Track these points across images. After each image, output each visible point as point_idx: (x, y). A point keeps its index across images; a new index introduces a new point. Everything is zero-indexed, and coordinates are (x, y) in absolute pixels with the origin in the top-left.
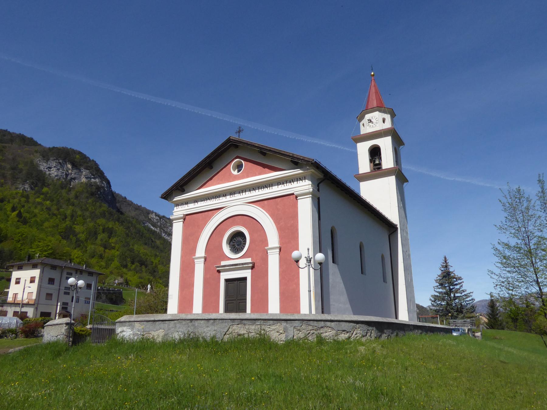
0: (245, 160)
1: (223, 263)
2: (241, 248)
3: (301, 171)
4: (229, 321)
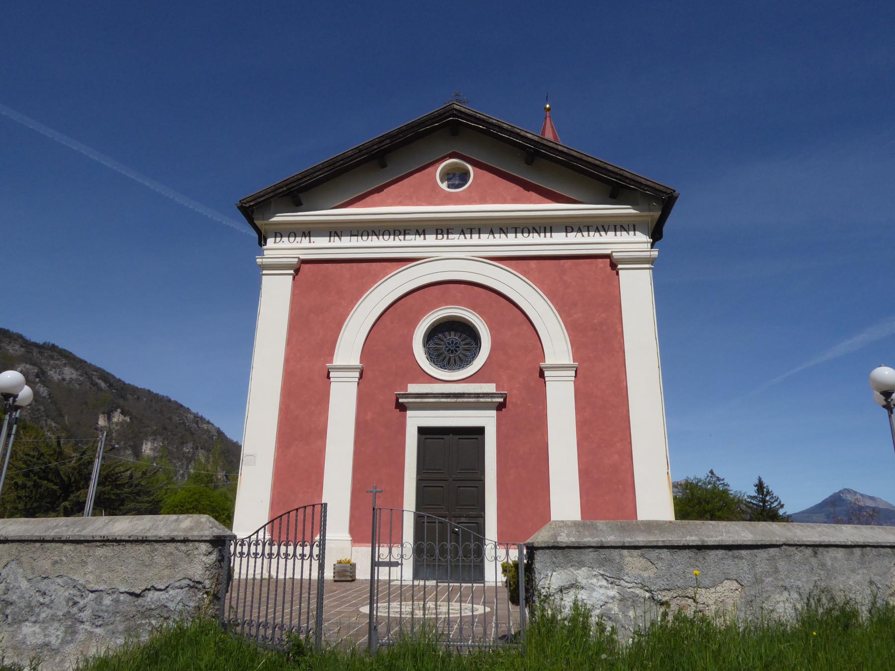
1: (413, 388)
2: (457, 358)
3: (632, 211)
4: (889, 550)
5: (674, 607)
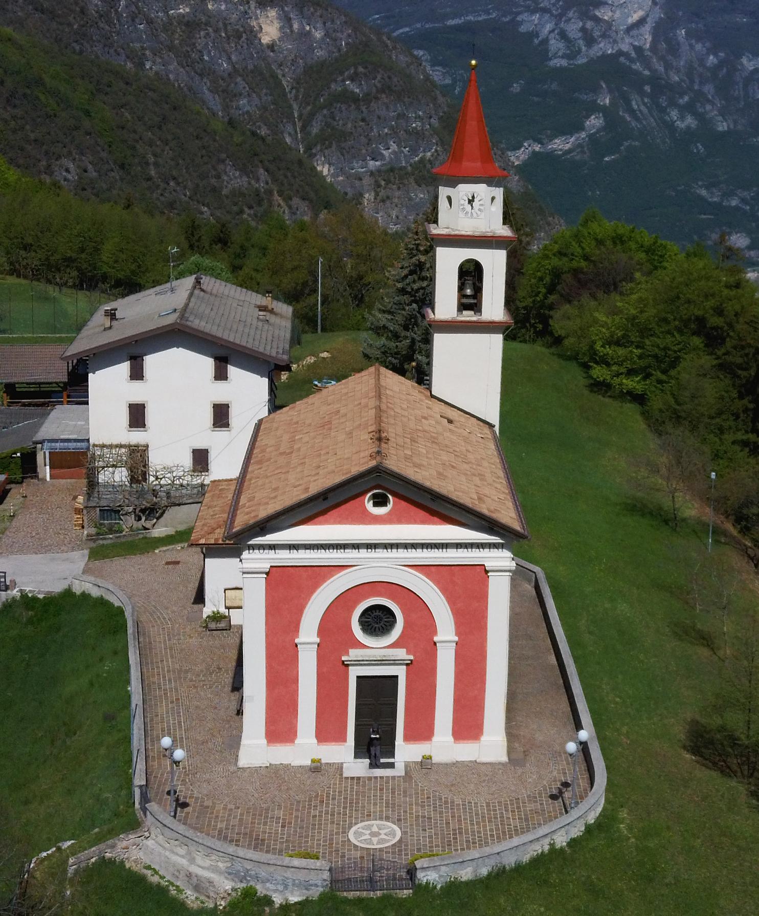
0: (395, 495)
5: (453, 877)
